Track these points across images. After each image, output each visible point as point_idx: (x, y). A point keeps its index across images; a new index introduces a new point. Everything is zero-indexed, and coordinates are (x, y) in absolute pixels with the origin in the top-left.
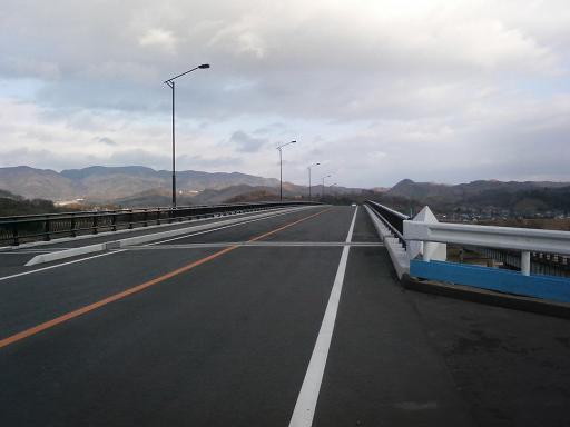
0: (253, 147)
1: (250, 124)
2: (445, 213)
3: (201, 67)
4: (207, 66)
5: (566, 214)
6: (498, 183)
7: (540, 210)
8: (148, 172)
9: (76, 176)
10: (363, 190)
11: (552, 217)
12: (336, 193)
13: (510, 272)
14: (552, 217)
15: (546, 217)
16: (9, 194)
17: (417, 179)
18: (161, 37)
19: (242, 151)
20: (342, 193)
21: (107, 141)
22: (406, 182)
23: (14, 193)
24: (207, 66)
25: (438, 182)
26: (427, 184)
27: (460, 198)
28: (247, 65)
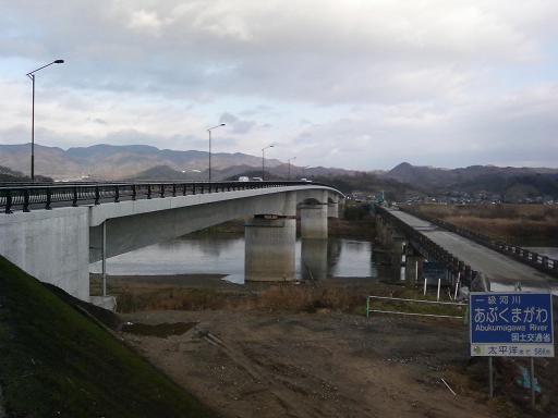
0: (243, 129)
1: (235, 104)
2: (435, 196)
3: (57, 62)
4: (61, 61)
5: (555, 200)
6: (494, 168)
7: (530, 195)
8: (154, 151)
9: (78, 154)
10: (357, 172)
11: (541, 203)
12: (330, 174)
13: (261, 213)
14: (541, 203)
15: (535, 203)
16: (9, 170)
17: (415, 163)
18: (146, 19)
19: (235, 132)
20: (335, 175)
21: (99, 121)
22: (405, 166)
23: (13, 170)
24: (61, 61)
25: (435, 165)
26: (425, 168)
27: (454, 183)
28: (227, 47)
